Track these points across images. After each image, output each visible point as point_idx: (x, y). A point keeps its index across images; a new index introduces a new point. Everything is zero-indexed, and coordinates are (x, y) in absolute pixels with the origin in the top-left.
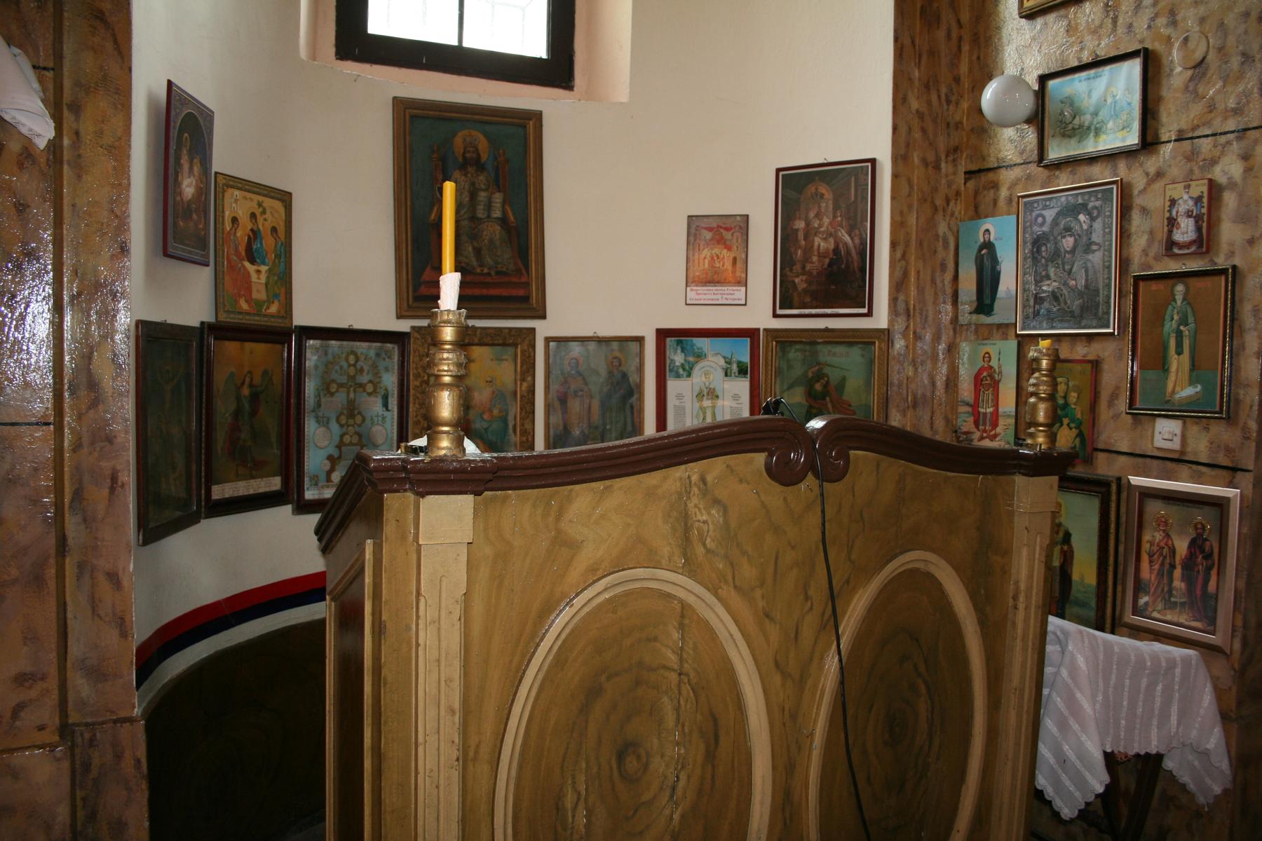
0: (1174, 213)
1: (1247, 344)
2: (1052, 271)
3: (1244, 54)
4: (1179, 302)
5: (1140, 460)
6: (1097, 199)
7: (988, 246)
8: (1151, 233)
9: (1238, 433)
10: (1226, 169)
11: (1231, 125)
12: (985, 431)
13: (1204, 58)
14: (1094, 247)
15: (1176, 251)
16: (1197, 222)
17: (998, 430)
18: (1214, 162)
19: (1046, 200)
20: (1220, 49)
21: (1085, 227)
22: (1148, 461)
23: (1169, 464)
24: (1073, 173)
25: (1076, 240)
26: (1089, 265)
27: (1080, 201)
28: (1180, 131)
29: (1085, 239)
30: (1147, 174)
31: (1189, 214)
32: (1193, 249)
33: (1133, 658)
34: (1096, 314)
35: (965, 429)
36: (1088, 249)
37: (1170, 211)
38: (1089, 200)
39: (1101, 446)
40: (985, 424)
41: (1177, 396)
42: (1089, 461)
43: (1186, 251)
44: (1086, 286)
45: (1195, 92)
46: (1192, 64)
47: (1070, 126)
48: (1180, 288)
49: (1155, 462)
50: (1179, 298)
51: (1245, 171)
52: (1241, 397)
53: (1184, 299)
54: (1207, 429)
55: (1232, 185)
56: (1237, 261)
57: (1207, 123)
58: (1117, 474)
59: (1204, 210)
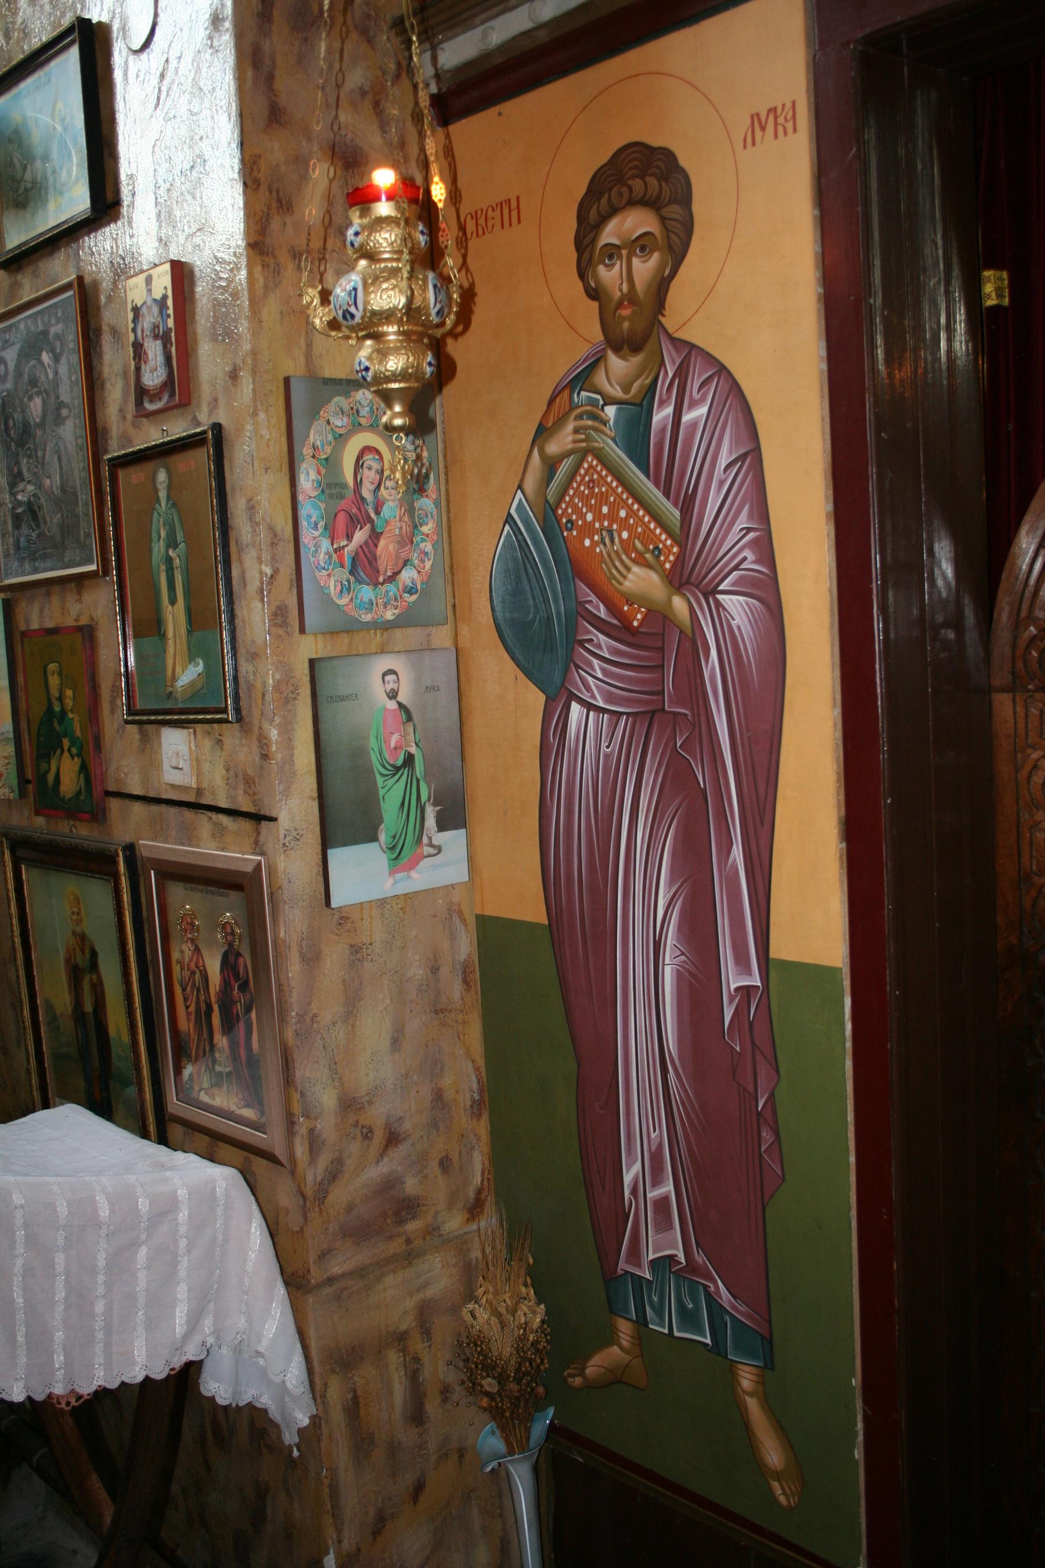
5: (156, 809)
15: (150, 407)
22: (164, 808)
33: (63, 1210)
39: (112, 787)
42: (98, 816)
49: (173, 811)
56: (222, 417)
58: (128, 839)
59: (171, 323)
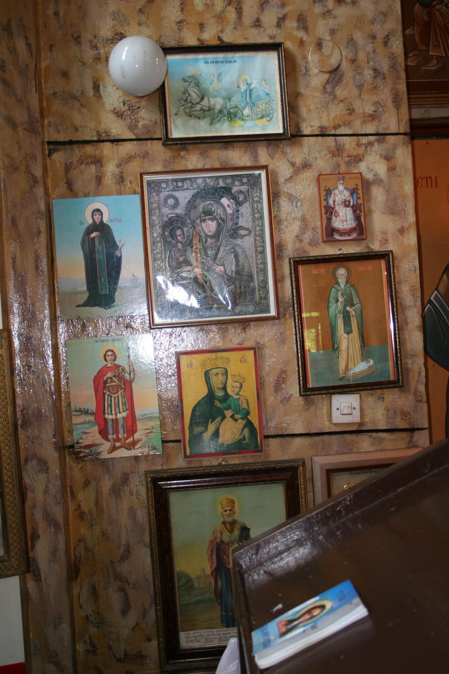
0: (331, 202)
1: (409, 320)
2: (192, 257)
3: (375, 70)
4: (342, 286)
5: (317, 439)
6: (243, 184)
7: (102, 228)
8: (303, 219)
9: (411, 398)
10: (371, 167)
11: (370, 128)
12: (118, 440)
13: (339, 65)
14: (242, 232)
15: (337, 237)
16: (354, 211)
17: (137, 436)
18: (358, 159)
19: (176, 181)
20: (353, 61)
21: (229, 211)
22: (326, 437)
23: (349, 437)
24: (203, 154)
25: (219, 225)
26: (239, 250)
27: (221, 184)
28: (322, 128)
29: (230, 223)
30: (293, 164)
31: (346, 204)
32: (354, 236)
34: (252, 300)
35: (86, 442)
36: (235, 233)
37: (326, 200)
38: (233, 183)
39: (272, 432)
40: (116, 431)
41: (351, 373)
43: (348, 238)
44: (238, 272)
45: (333, 93)
46: (330, 69)
47: (198, 107)
48: (342, 272)
49: (334, 437)
50: (342, 281)
51: (388, 170)
52: (410, 366)
53: (347, 282)
54: (382, 398)
55: (378, 181)
56: (390, 247)
57: (348, 124)
